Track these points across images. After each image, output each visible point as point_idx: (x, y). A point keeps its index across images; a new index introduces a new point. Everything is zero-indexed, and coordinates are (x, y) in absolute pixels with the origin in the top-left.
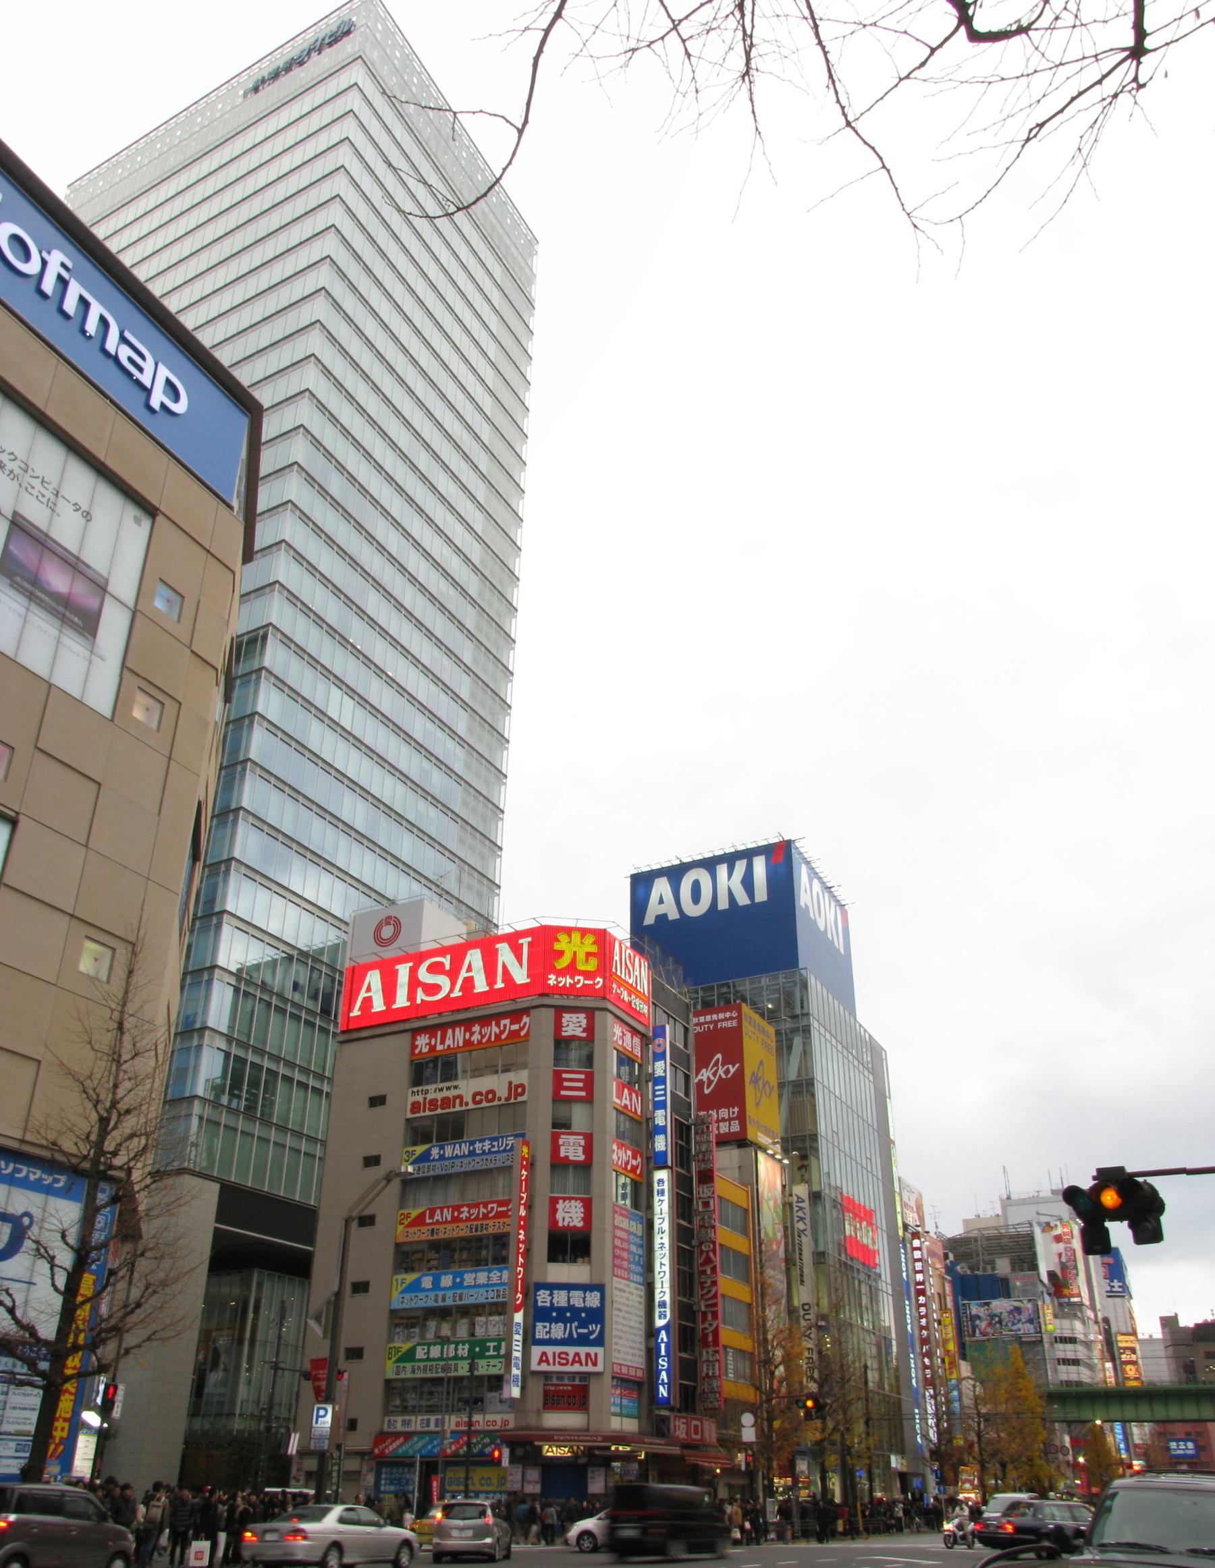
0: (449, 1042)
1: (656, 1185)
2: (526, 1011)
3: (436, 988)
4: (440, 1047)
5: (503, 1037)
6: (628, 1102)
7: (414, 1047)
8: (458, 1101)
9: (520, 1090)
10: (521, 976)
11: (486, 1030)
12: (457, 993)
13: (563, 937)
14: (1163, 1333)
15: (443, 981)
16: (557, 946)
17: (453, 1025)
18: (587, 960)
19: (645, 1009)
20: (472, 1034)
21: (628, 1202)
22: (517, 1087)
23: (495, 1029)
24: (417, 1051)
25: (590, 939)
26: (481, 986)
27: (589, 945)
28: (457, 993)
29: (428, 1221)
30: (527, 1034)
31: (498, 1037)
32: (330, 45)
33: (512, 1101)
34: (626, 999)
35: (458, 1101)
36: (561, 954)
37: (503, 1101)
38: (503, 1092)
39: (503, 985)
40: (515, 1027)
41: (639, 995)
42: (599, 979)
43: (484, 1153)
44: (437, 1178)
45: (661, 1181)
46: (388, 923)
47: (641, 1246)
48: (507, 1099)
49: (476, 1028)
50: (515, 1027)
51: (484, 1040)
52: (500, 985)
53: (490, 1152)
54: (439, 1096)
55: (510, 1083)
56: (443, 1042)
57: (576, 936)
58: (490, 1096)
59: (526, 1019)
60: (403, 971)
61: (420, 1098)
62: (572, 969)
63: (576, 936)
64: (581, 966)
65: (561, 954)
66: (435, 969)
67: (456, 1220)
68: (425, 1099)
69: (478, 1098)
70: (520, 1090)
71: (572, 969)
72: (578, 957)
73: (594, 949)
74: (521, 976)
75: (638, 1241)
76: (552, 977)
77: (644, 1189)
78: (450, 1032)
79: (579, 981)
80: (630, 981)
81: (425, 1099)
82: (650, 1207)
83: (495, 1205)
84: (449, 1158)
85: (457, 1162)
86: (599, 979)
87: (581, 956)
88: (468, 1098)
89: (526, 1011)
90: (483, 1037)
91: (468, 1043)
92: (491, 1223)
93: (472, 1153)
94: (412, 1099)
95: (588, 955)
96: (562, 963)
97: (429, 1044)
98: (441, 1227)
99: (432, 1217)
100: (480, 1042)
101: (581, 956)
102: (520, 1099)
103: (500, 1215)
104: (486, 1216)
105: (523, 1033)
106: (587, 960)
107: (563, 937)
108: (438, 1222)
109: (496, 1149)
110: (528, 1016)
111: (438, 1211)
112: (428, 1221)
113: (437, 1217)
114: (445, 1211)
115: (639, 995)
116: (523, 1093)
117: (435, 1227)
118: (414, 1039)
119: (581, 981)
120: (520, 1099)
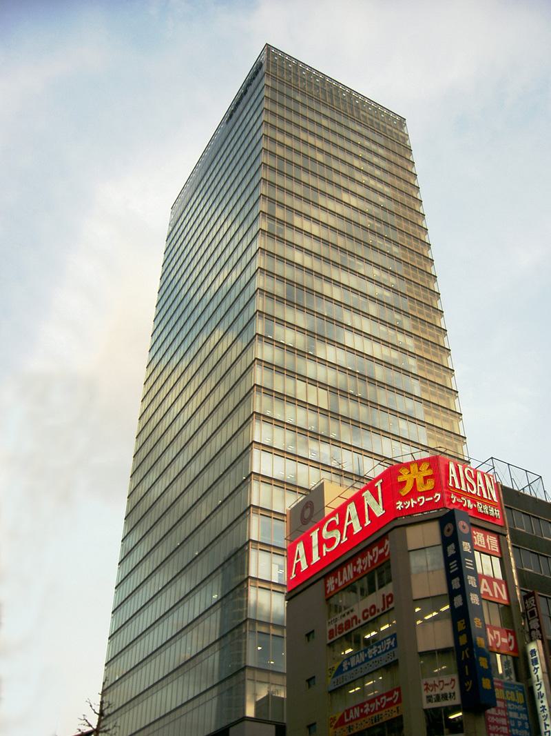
0: (345, 578)
1: (530, 656)
2: (385, 536)
3: (333, 540)
4: (340, 584)
5: (375, 561)
6: (488, 590)
7: (326, 588)
8: (354, 621)
9: (390, 599)
10: (379, 511)
11: (365, 561)
12: (345, 539)
13: (404, 471)
14: (481, 681)
15: (336, 533)
16: (400, 479)
17: (345, 564)
18: (425, 483)
19: (495, 512)
20: (357, 566)
21: (513, 676)
22: (388, 597)
23: (370, 557)
24: (328, 592)
25: (425, 466)
26: (357, 528)
27: (426, 471)
28: (345, 539)
29: (346, 720)
30: (389, 555)
31: (372, 562)
32: (256, 75)
33: (386, 609)
34: (470, 506)
35: (354, 621)
36: (404, 483)
37: (381, 612)
38: (380, 606)
39: (370, 522)
40: (382, 551)
41: (490, 503)
42: (436, 495)
43: (374, 657)
44: (340, 687)
45: (533, 652)
46: (307, 507)
47: (525, 712)
48: (383, 609)
49: (359, 561)
50: (382, 551)
51: (365, 568)
52: (368, 522)
53: (378, 655)
54: (343, 621)
55: (383, 596)
56: (342, 580)
57: (414, 468)
58: (373, 610)
59: (387, 542)
60: (315, 535)
61: (332, 627)
62: (414, 493)
63: (414, 468)
64: (421, 489)
65: (404, 483)
66: (332, 527)
67: (363, 715)
68: (336, 625)
69: (365, 614)
70: (390, 599)
71: (414, 493)
72: (418, 482)
73: (430, 472)
74: (379, 511)
75: (522, 708)
76: (400, 503)
77: (521, 661)
78: (345, 569)
79: (421, 500)
80: (474, 492)
81: (336, 625)
82: (528, 675)
83: (384, 697)
84: (354, 667)
85: (359, 668)
86: (436, 495)
87: (420, 481)
88: (360, 617)
89: (385, 536)
90: (363, 566)
91: (355, 574)
92: (383, 712)
93: (367, 659)
94: (329, 628)
95: (425, 478)
96: (407, 489)
97: (334, 584)
98: (354, 723)
99: (348, 717)
100: (362, 571)
101: (420, 481)
102: (391, 606)
103: (390, 704)
104: (380, 708)
105: (386, 554)
106: (425, 483)
107: (404, 471)
108: (352, 720)
109: (380, 652)
110: (388, 539)
111: (351, 711)
112: (346, 720)
113: (351, 716)
114: (355, 709)
115: (490, 503)
116: (391, 602)
117: (351, 724)
118: (326, 583)
119: (423, 500)
120: (391, 606)
